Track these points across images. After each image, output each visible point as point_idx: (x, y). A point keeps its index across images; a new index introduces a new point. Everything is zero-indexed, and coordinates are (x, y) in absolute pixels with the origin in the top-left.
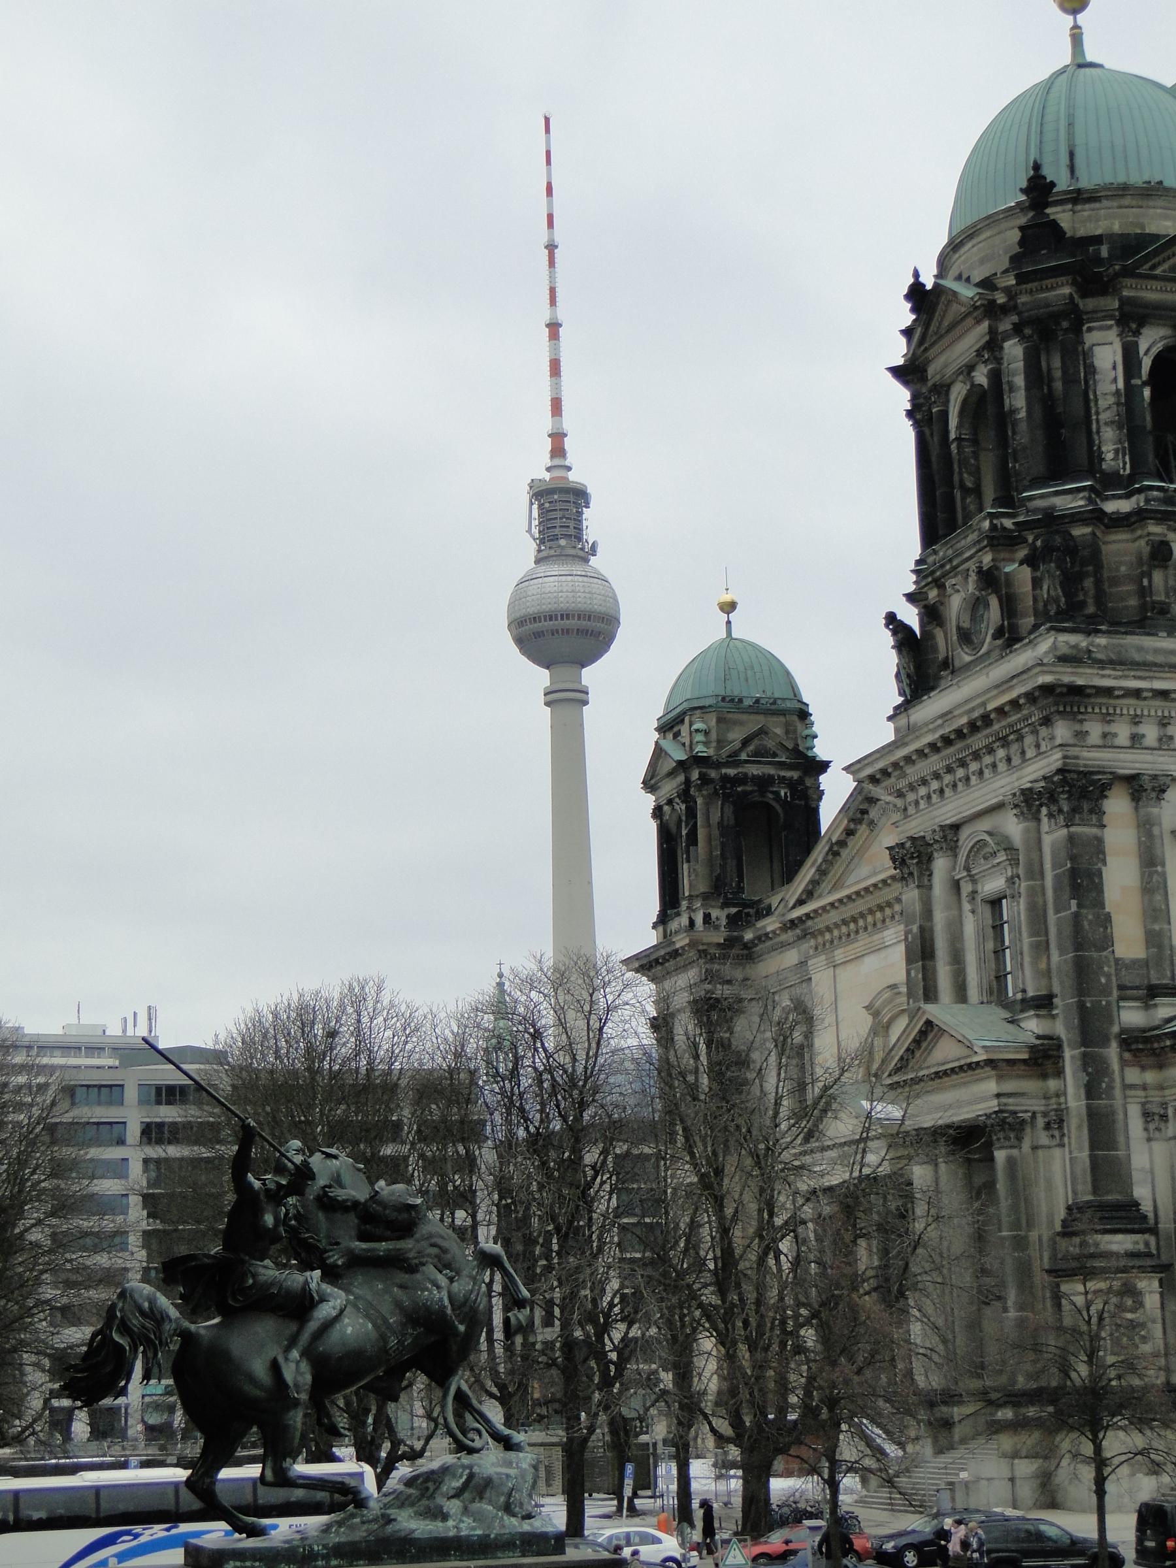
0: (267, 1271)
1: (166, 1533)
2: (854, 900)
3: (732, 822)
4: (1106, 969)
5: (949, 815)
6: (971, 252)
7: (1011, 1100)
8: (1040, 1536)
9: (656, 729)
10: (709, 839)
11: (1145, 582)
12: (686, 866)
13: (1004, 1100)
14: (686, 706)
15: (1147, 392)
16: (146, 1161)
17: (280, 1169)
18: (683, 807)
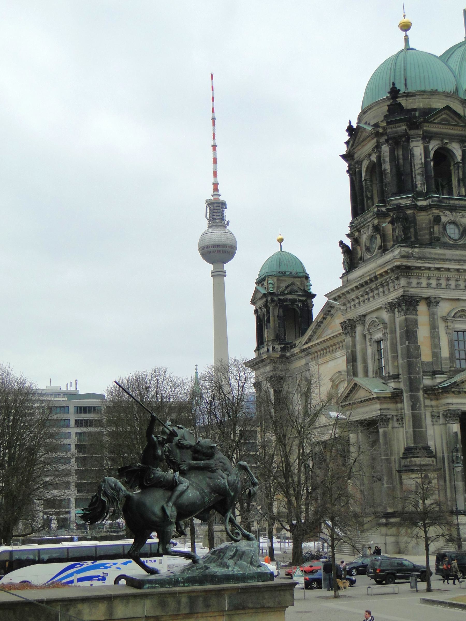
0: (159, 472)
1: (92, 564)
2: (325, 342)
3: (282, 315)
4: (418, 365)
5: (362, 311)
6: (370, 114)
7: (385, 411)
8: (401, 564)
9: (256, 283)
10: (274, 321)
11: (432, 230)
12: (266, 330)
13: (382, 411)
14: (266, 275)
15: (432, 163)
16: (76, 433)
17: (163, 433)
18: (265, 310)
